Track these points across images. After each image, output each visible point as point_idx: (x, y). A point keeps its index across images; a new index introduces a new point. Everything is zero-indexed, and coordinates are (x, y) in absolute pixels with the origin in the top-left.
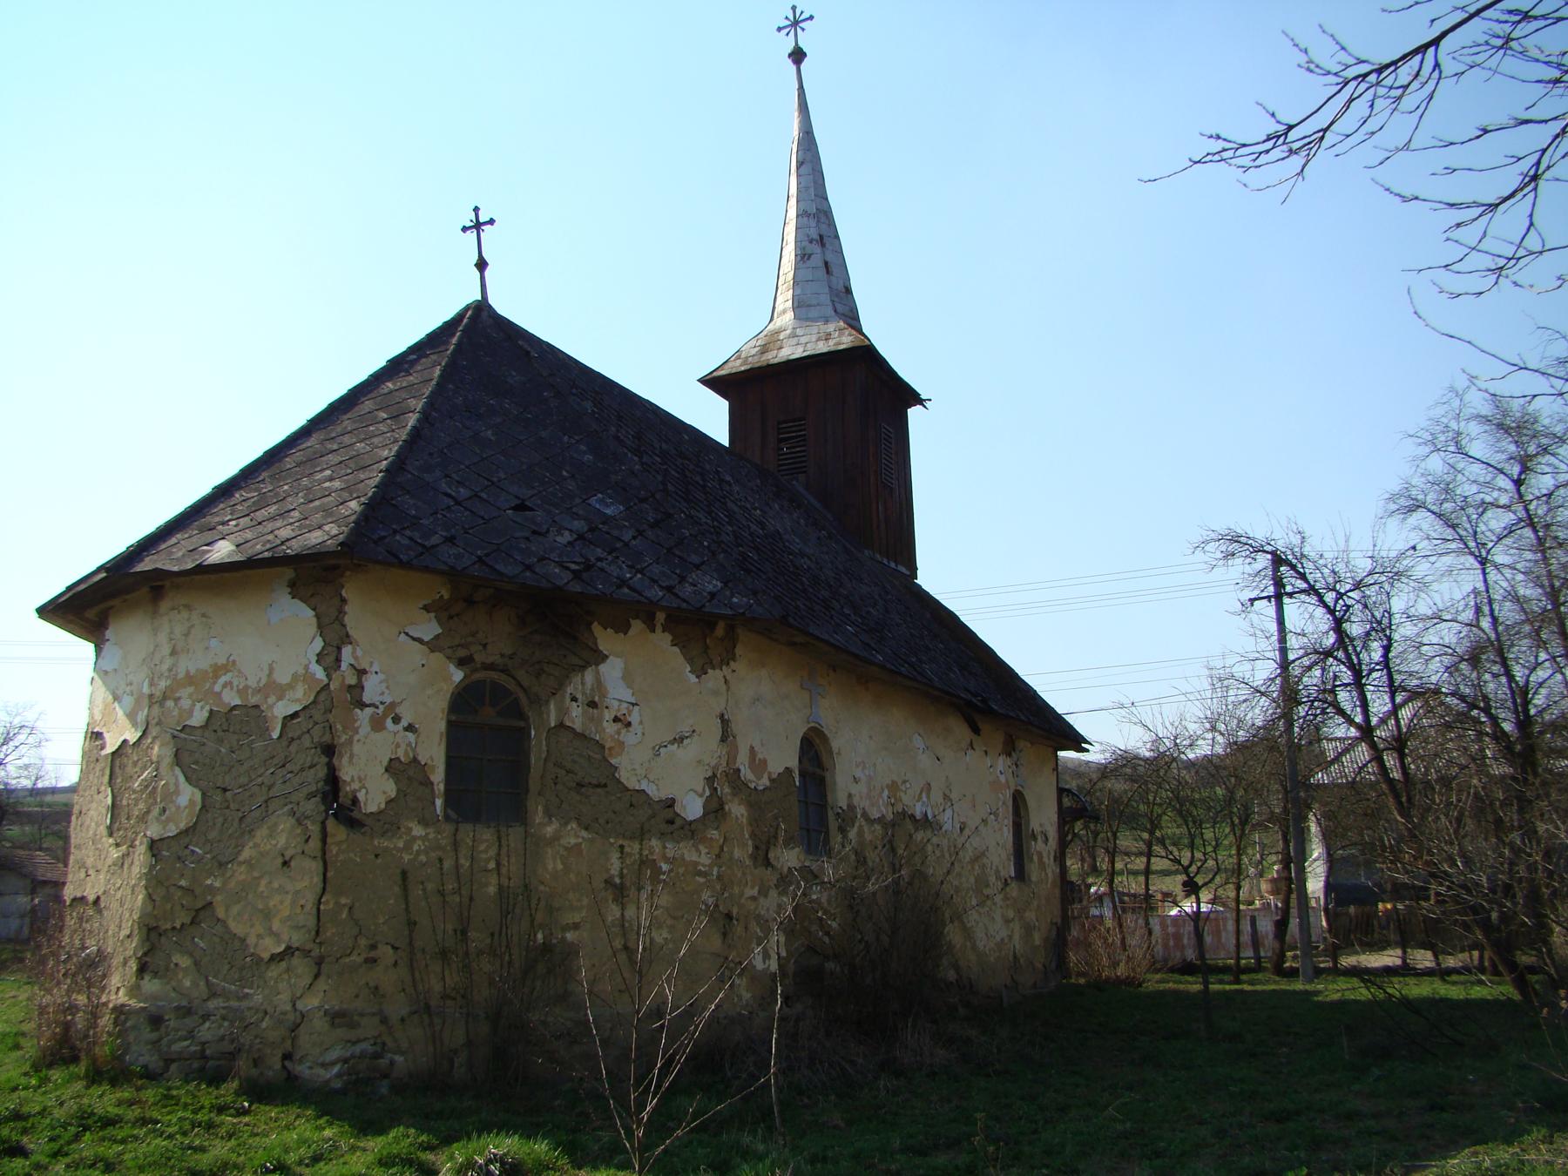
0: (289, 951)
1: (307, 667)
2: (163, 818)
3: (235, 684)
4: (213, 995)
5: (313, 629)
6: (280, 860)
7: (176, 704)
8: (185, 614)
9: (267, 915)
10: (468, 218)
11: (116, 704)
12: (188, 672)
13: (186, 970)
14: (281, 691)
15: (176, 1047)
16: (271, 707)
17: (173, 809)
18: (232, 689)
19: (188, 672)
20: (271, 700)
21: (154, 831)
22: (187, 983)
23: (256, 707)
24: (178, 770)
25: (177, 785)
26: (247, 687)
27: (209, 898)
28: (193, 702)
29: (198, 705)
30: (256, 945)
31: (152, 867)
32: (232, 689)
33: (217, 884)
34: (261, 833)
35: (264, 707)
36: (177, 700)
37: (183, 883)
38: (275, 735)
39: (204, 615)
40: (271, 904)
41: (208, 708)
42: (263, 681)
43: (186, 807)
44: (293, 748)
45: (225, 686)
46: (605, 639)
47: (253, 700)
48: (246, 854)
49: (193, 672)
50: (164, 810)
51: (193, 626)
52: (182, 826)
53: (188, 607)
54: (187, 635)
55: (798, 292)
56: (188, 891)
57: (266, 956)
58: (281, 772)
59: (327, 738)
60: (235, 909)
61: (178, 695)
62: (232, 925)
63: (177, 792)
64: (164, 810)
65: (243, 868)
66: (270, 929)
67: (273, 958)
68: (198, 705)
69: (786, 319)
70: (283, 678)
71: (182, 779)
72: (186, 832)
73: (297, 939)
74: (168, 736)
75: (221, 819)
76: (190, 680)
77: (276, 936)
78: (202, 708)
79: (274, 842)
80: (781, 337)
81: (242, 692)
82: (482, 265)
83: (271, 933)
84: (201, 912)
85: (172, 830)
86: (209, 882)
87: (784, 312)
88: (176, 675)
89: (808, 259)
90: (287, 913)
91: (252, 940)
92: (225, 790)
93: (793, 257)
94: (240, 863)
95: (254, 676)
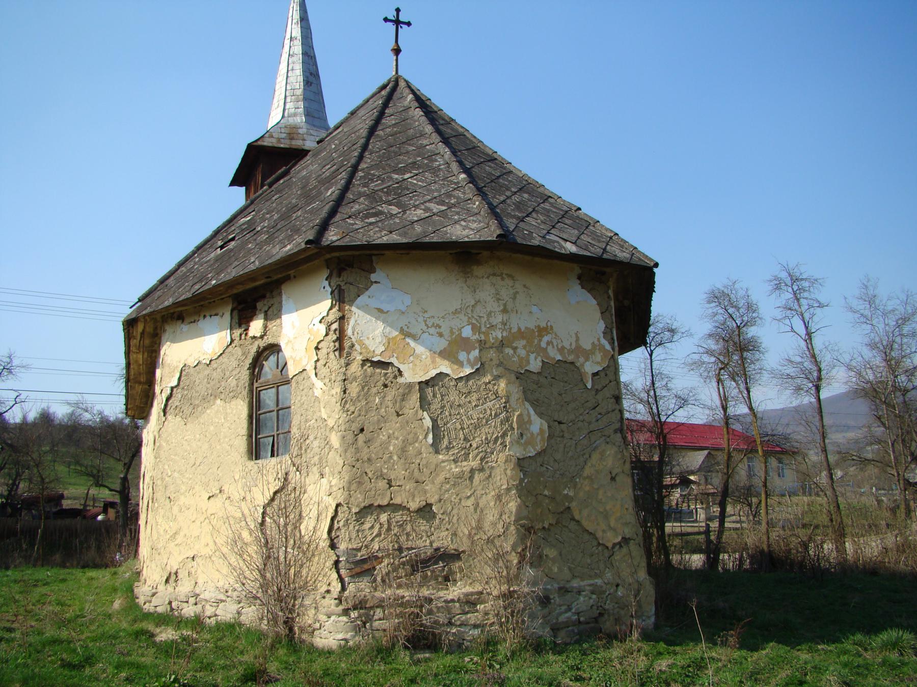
0: (626, 540)
1: (599, 340)
2: (523, 441)
3: (555, 344)
4: (574, 577)
5: (598, 315)
6: (609, 477)
7: (515, 352)
8: (508, 282)
9: (606, 516)
10: (392, 15)
11: (408, 340)
12: (519, 329)
13: (554, 560)
14: (587, 355)
15: (562, 618)
16: (583, 365)
17: (529, 435)
18: (553, 347)
19: (519, 329)
20: (582, 360)
21: (519, 452)
22: (556, 570)
23: (572, 363)
24: (527, 405)
25: (529, 415)
26: (563, 348)
27: (567, 504)
28: (528, 352)
29: (532, 356)
30: (603, 538)
31: (521, 480)
32: (553, 347)
33: (571, 494)
34: (595, 456)
35: (578, 364)
36: (515, 349)
37: (546, 493)
38: (589, 386)
39: (525, 286)
40: (608, 508)
41: (539, 359)
42: (573, 347)
43: (538, 434)
44: (600, 397)
45: (548, 343)
46: (749, 335)
47: (571, 358)
48: (587, 471)
49: (523, 329)
50: (522, 435)
51: (517, 293)
52: (539, 448)
53: (510, 276)
54: (514, 298)
55: (307, 105)
56: (552, 498)
57: (610, 545)
58: (594, 413)
59: (617, 393)
60: (585, 512)
61: (514, 345)
62: (585, 523)
63: (530, 422)
64: (522, 435)
65: (586, 482)
66: (609, 526)
67: (614, 545)
68: (532, 356)
69: (300, 119)
70: (587, 345)
71: (532, 412)
72: (539, 454)
73: (628, 532)
74: (513, 377)
75: (562, 446)
76: (521, 334)
77: (614, 530)
78: (536, 359)
79: (605, 463)
80: (300, 131)
81: (561, 350)
82: (397, 51)
83: (610, 528)
84: (564, 514)
85: (532, 453)
86: (566, 492)
87: (295, 115)
88: (511, 329)
89: (311, 85)
90: (619, 514)
91: (599, 534)
92: (560, 423)
93: (301, 79)
94: (585, 479)
95: (568, 342)
